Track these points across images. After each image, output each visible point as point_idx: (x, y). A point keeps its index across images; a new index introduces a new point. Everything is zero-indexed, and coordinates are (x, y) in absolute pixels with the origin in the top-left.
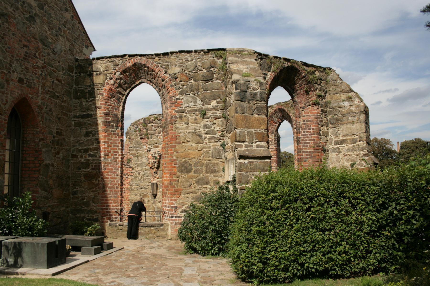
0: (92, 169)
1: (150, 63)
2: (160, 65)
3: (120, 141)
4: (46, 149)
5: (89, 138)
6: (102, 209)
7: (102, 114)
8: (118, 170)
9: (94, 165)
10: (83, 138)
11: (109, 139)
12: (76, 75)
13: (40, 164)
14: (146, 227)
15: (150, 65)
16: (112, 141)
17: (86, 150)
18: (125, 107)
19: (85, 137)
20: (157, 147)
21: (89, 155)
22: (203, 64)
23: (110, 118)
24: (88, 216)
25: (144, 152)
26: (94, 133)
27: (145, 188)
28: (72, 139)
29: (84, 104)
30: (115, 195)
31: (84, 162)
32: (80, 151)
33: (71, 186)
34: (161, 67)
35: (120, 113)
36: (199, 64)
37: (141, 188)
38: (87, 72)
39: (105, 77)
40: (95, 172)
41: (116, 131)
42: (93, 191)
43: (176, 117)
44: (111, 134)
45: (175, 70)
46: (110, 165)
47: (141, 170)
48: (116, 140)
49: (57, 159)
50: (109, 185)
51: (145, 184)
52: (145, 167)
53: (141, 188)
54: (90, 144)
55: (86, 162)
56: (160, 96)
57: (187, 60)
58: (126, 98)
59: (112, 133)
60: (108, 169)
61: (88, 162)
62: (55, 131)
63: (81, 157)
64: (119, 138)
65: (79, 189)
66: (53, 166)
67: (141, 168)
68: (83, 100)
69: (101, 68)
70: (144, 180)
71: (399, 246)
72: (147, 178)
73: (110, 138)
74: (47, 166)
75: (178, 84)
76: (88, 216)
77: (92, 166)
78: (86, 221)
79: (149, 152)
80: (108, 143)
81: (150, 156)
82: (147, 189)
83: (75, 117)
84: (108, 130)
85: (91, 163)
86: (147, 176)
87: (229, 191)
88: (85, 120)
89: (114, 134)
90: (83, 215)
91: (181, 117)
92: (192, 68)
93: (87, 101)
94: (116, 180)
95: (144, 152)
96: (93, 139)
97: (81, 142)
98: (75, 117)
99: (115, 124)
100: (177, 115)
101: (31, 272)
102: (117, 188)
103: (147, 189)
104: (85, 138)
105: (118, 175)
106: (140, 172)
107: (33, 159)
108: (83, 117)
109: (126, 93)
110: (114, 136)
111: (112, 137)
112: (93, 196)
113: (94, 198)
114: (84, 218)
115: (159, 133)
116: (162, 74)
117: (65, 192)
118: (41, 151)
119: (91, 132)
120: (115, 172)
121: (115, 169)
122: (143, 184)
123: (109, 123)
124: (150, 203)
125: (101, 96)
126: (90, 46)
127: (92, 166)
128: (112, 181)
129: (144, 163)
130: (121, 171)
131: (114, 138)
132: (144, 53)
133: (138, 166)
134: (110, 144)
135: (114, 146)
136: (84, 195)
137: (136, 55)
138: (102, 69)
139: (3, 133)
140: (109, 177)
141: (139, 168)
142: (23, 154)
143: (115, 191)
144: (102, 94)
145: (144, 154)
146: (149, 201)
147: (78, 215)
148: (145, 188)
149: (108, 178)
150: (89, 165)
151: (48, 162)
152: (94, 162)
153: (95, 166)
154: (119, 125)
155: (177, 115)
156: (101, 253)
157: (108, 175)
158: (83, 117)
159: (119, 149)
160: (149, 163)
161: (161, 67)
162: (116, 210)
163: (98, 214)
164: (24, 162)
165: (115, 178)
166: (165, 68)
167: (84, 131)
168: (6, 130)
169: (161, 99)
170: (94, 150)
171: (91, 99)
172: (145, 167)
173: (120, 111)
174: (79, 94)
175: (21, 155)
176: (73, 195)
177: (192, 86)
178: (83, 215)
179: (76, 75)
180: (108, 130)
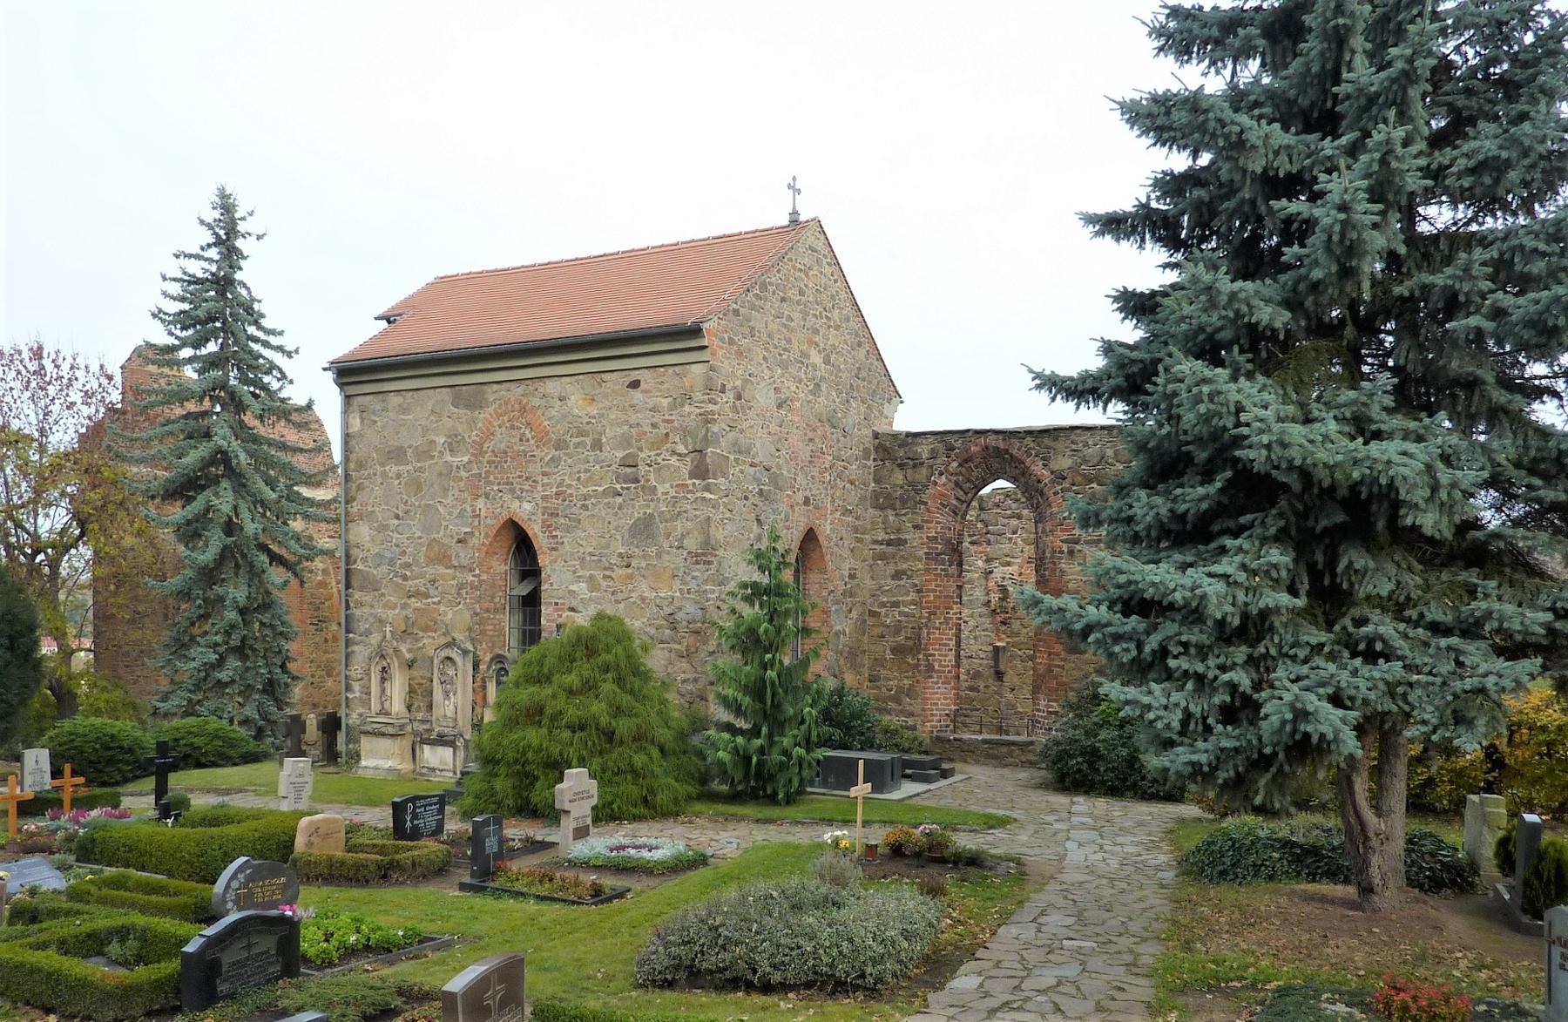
1: (1016, 449)
10: (889, 581)
15: (1015, 452)
17: (896, 604)
20: (1008, 564)
21: (901, 613)
22: (1116, 453)
28: (868, 582)
32: (883, 605)
36: (1110, 452)
40: (910, 643)
43: (1062, 552)
45: (1063, 463)
47: (971, 616)
57: (1086, 445)
62: (846, 573)
63: (887, 616)
68: (890, 512)
71: (63, 545)
74: (837, 634)
75: (1068, 490)
81: (991, 584)
83: (875, 542)
87: (1324, 613)
91: (1071, 552)
92: (1095, 461)
98: (875, 542)
100: (1065, 548)
108: (889, 543)
116: (1038, 469)
119: (904, 573)
122: (976, 647)
124: (990, 690)
126: (893, 394)
155: (1065, 548)
158: (889, 543)
167: (891, 569)
177: (1093, 495)
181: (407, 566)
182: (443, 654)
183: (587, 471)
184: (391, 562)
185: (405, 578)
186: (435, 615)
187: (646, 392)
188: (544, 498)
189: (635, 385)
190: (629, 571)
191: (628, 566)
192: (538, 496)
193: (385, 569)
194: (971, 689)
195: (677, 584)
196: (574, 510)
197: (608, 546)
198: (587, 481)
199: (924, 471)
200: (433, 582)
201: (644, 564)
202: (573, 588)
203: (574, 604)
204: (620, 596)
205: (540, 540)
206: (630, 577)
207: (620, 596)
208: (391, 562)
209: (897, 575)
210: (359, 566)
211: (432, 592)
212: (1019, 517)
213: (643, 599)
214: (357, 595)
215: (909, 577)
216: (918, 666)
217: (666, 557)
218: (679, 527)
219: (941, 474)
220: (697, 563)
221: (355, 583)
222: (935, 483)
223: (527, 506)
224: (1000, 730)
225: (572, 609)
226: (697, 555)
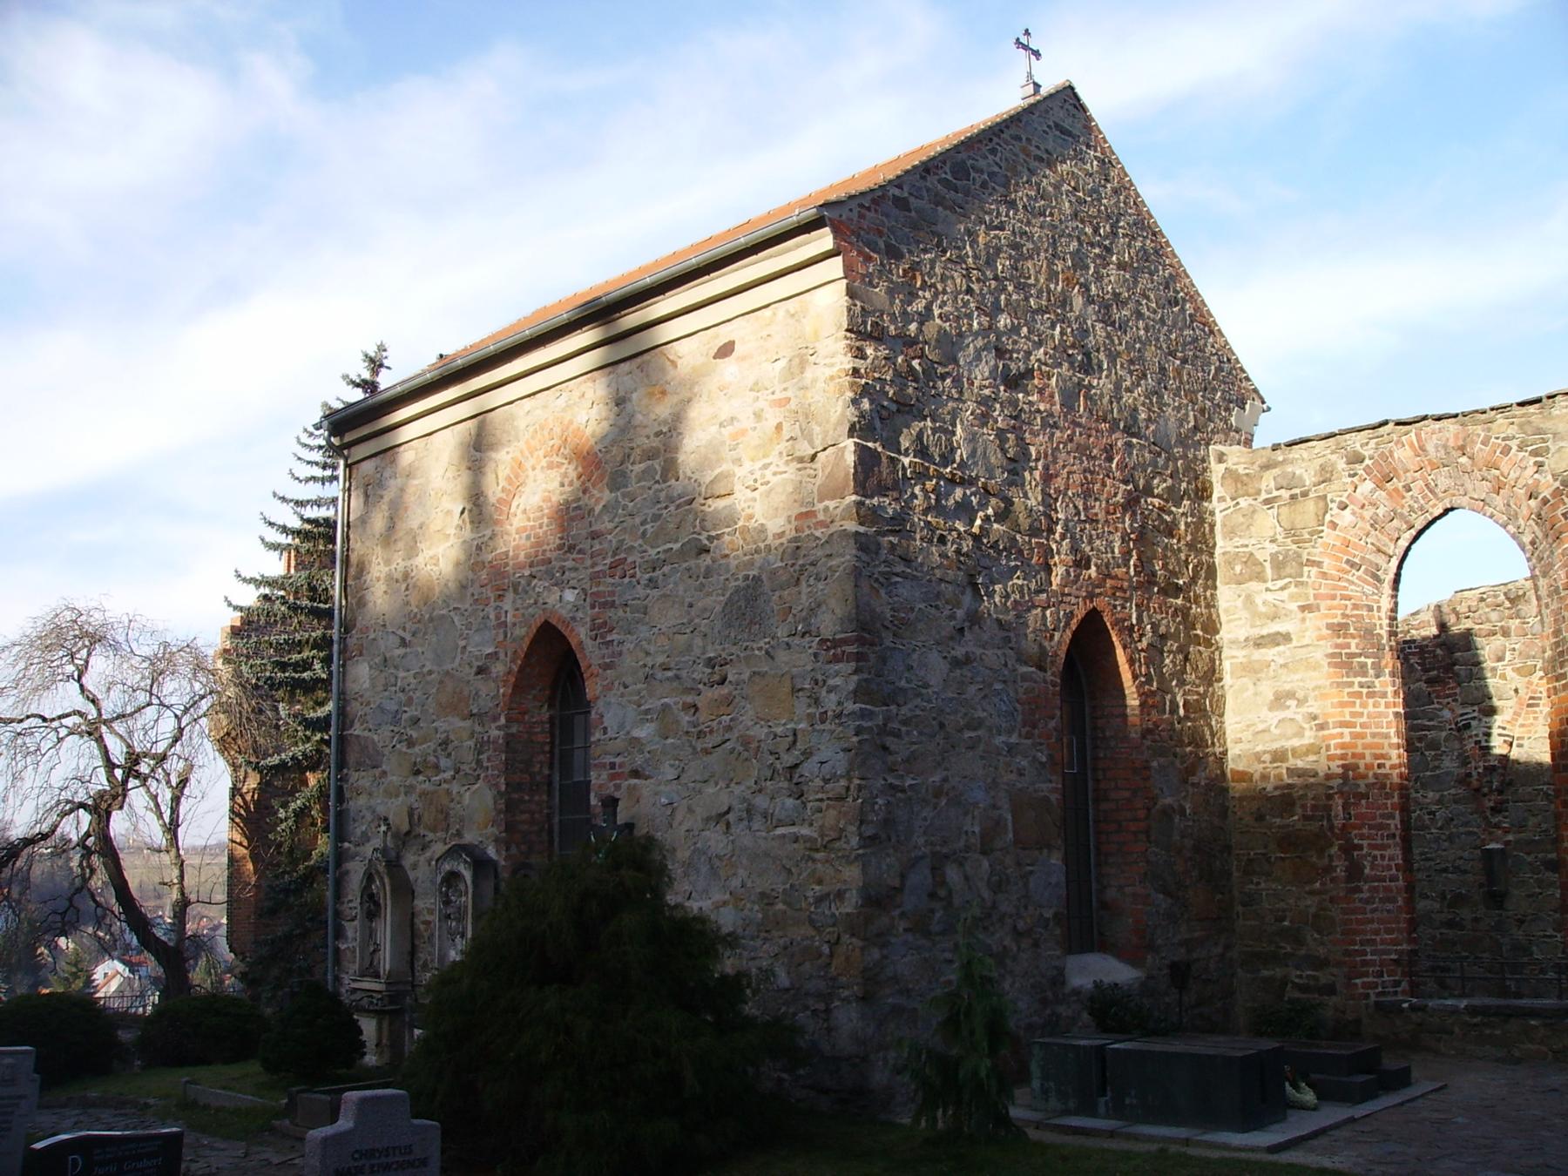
0: (1305, 818)
2: (1514, 444)
3: (1391, 717)
4: (1162, 760)
5: (1288, 714)
6: (1347, 953)
7: (1325, 632)
8: (1392, 817)
9: (1310, 803)
11: (1353, 714)
12: (1223, 505)
13: (1149, 809)
14: (1510, 1016)
16: (1364, 719)
18: (1399, 599)
19: (1270, 709)
23: (1353, 643)
24: (1300, 977)
25: (1444, 734)
26: (1300, 694)
27: (1457, 870)
29: (1259, 601)
30: (1390, 906)
31: (1277, 793)
33: (1236, 874)
34: (1520, 449)
35: (1386, 622)
37: (1445, 870)
38: (1259, 492)
39: (1321, 504)
40: (1314, 826)
41: (1377, 682)
42: (1311, 893)
44: (1359, 695)
46: (1363, 802)
47: (1439, 802)
48: (1380, 715)
49: (1191, 790)
50: (1367, 871)
51: (1460, 853)
52: (1453, 791)
53: (1445, 870)
54: (1290, 732)
55: (1283, 795)
56: (1523, 549)
58: (1400, 567)
59: (1365, 691)
60: (1360, 816)
61: (1290, 795)
64: (1387, 705)
65: (1263, 885)
66: (1182, 811)
67: (1437, 796)
68: (1254, 586)
69: (1306, 476)
70: (1450, 839)
72: (1462, 830)
73: (1358, 709)
74: (1167, 813)
76: (1300, 977)
77: (1304, 807)
78: (1297, 995)
79: (1466, 734)
80: (1353, 725)
82: (1465, 872)
84: (1351, 684)
85: (1301, 797)
86: (1466, 824)
88: (1269, 653)
89: (1371, 695)
90: (1279, 972)
93: (1267, 590)
94: (1387, 853)
95: (1444, 734)
96: (1299, 718)
97: (1261, 727)
99: (1369, 661)
101: (1208, 1137)
102: (1393, 879)
103: (1465, 872)
104: (1271, 715)
105: (1394, 836)
106: (1434, 808)
107: (1127, 794)
109: (1400, 552)
110: (1371, 701)
111: (1364, 705)
112: (1313, 910)
113: (1316, 916)
114: (1284, 982)
115: (1500, 659)
117: (1219, 896)
118: (1147, 768)
119: (1291, 695)
120: (1381, 827)
121: (1382, 816)
123: (1351, 656)
125: (1314, 570)
127: (1304, 807)
128: (1375, 858)
129: (1447, 773)
130: (1402, 821)
131: (1371, 708)
132: (1454, 412)
133: (1424, 786)
134: (1358, 729)
135: (1374, 735)
136: (1282, 905)
137: (1425, 418)
138: (1309, 479)
139: (1052, 724)
140: (1365, 843)
141: (1431, 794)
142: (1097, 781)
143: (1387, 889)
144: (1319, 564)
145: (1446, 740)
146: (1476, 920)
147: (1265, 973)
148: (1457, 870)
149: (1360, 847)
150: (1293, 804)
151: (1168, 801)
152: (1310, 795)
153: (1314, 807)
154: (1383, 663)
156: (1377, 1096)
157: (1362, 837)
159: (1390, 745)
160: (1469, 775)
161: (1520, 449)
162: (1394, 957)
163: (1335, 970)
164: (1104, 806)
165: (1383, 847)
166: (1535, 453)
167: (1267, 690)
168: (1058, 713)
169: (1529, 560)
170: (1307, 754)
171: (1281, 583)
172: (1453, 791)
173: (1383, 615)
174: (1238, 568)
175: (1090, 784)
176: (1244, 905)
178: (1279, 972)
179: (1223, 505)
180: (1351, 684)
181: (415, 721)
182: (447, 867)
183: (656, 517)
184: (395, 718)
185: (411, 743)
186: (445, 801)
187: (743, 358)
188: (595, 577)
189: (726, 350)
190: (725, 690)
191: (722, 682)
192: (584, 574)
193: (386, 731)
194: (1450, 924)
195: (802, 707)
196: (640, 591)
197: (689, 648)
198: (656, 535)
199: (1310, 506)
200: (445, 743)
201: (746, 676)
202: (636, 733)
203: (639, 760)
204: (710, 741)
205: (590, 653)
206: (729, 701)
207: (710, 741)
208: (395, 718)
209: (1280, 700)
210: (357, 730)
211: (443, 762)
212: (1506, 633)
213: (746, 742)
214: (354, 776)
215: (1301, 703)
216: (1329, 869)
217: (782, 656)
218: (804, 596)
219: (1344, 507)
220: (836, 659)
221: (352, 758)
222: (1334, 525)
223: (570, 596)
224: (1504, 992)
225: (636, 774)
226: (836, 643)
